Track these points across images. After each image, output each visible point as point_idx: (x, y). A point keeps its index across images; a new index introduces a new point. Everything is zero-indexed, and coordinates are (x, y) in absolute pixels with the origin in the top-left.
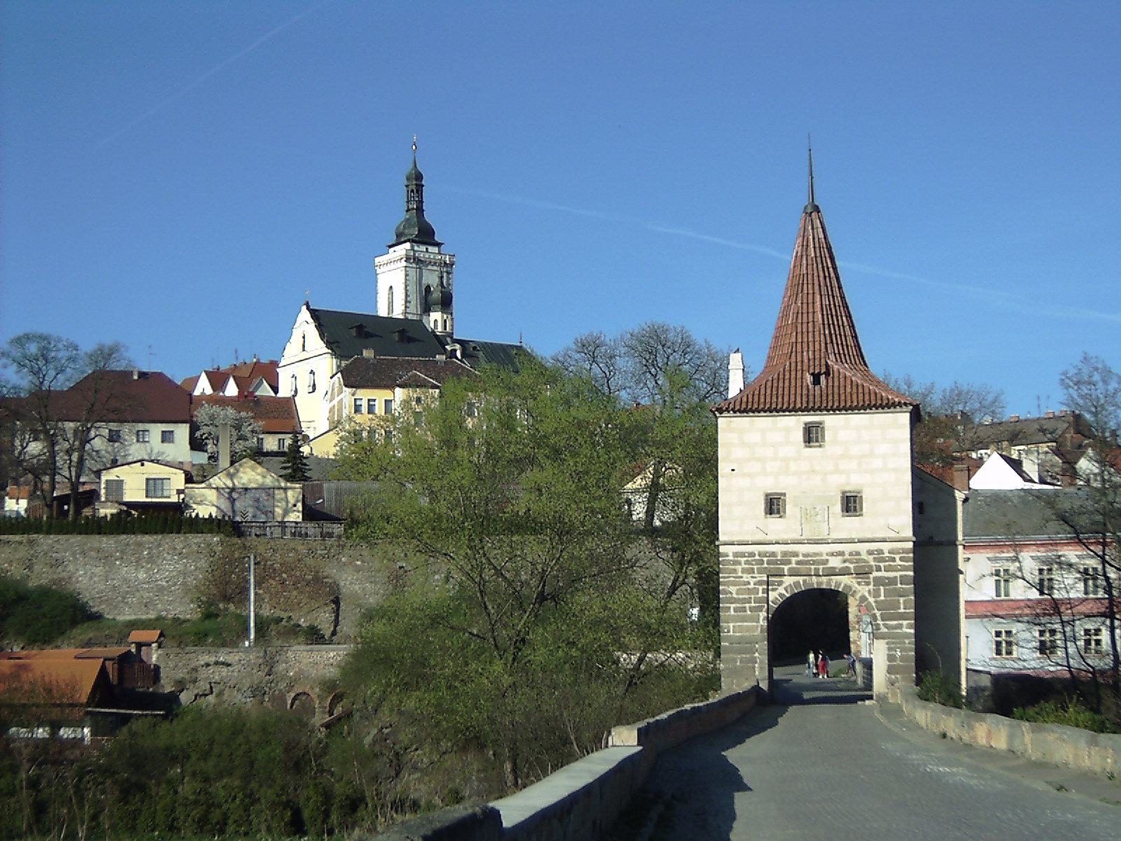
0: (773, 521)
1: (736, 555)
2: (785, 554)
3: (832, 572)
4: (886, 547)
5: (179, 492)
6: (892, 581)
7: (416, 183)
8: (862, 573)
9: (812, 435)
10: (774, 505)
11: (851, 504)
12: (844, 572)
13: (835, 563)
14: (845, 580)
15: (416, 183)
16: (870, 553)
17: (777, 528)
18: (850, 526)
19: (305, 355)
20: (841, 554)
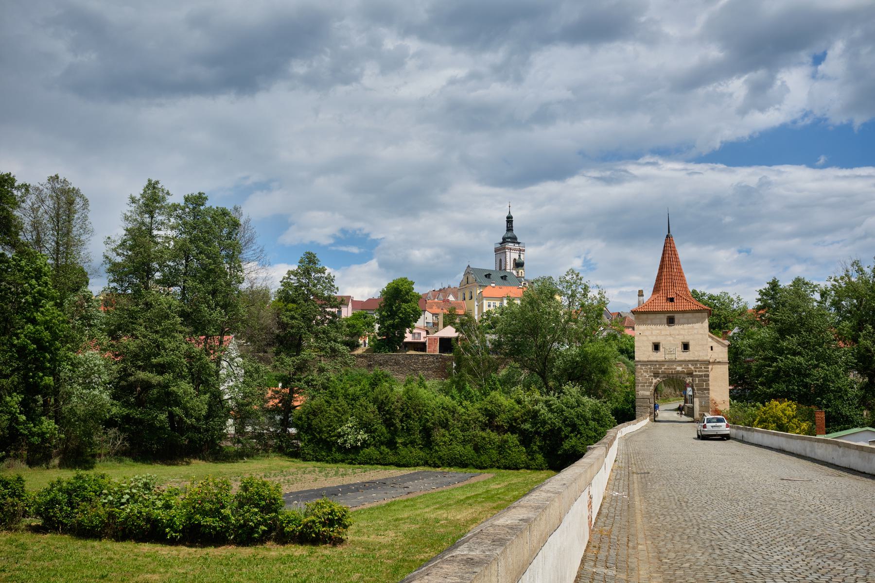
6: (701, 376)
10: (656, 347)
11: (686, 347)
17: (659, 356)
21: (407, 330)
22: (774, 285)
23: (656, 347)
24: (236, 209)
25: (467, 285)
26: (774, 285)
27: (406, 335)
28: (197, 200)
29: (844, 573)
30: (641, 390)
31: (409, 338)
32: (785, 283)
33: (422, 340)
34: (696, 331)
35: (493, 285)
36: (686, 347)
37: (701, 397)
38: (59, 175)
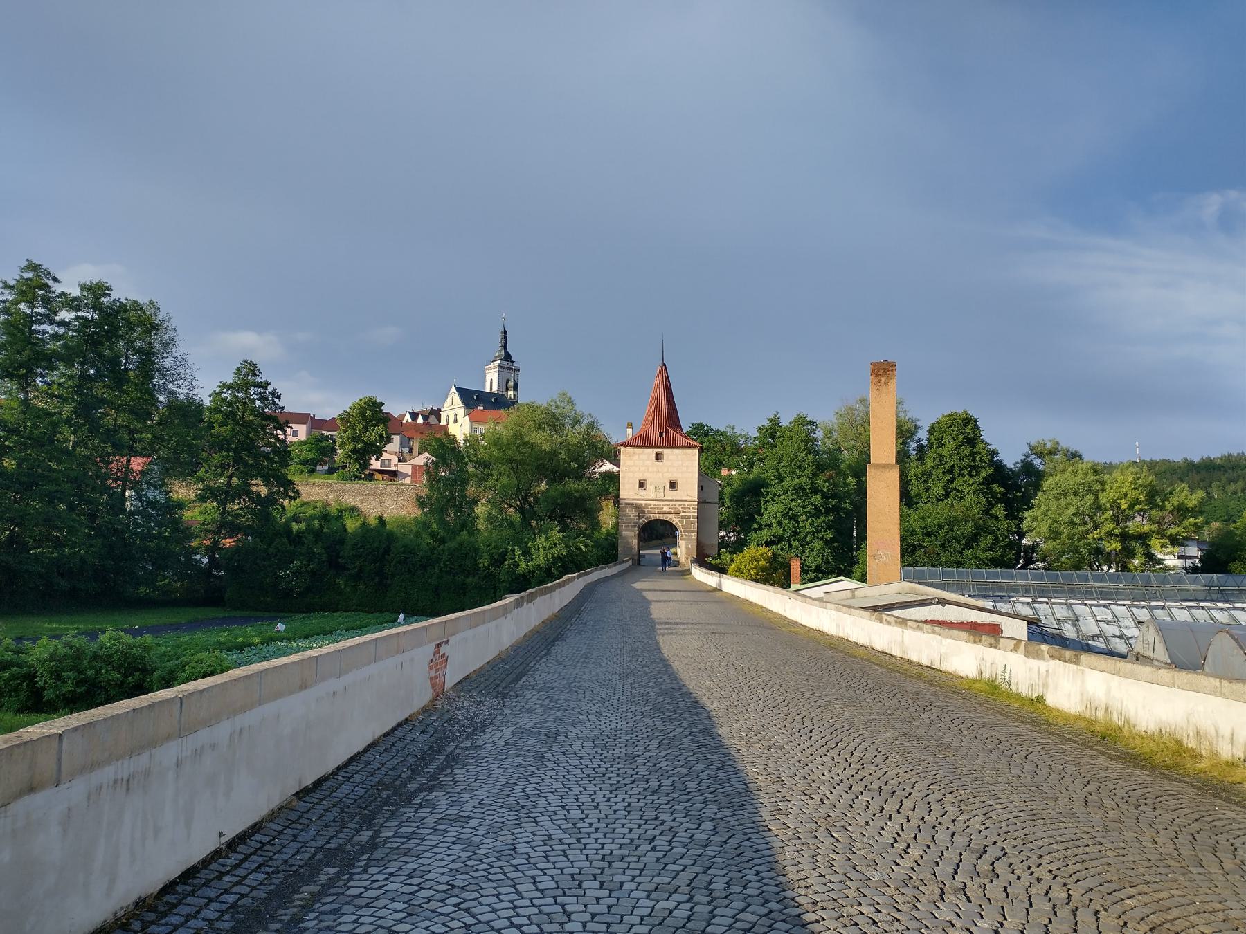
2: (646, 504)
3: (664, 513)
4: (686, 503)
5: (395, 466)
6: (689, 517)
8: (677, 513)
10: (642, 485)
12: (670, 513)
13: (666, 509)
14: (670, 516)
16: (680, 505)
18: (671, 494)
19: (453, 407)
20: (668, 505)
21: (374, 458)
22: (775, 422)
23: (642, 485)
24: (152, 303)
25: (453, 407)
26: (775, 422)
27: (371, 462)
28: (98, 290)
29: (646, 804)
30: (626, 530)
31: (375, 465)
32: (786, 420)
33: (393, 469)
34: (685, 469)
35: (481, 408)
36: (673, 485)
37: (688, 540)
38: (36, 261)
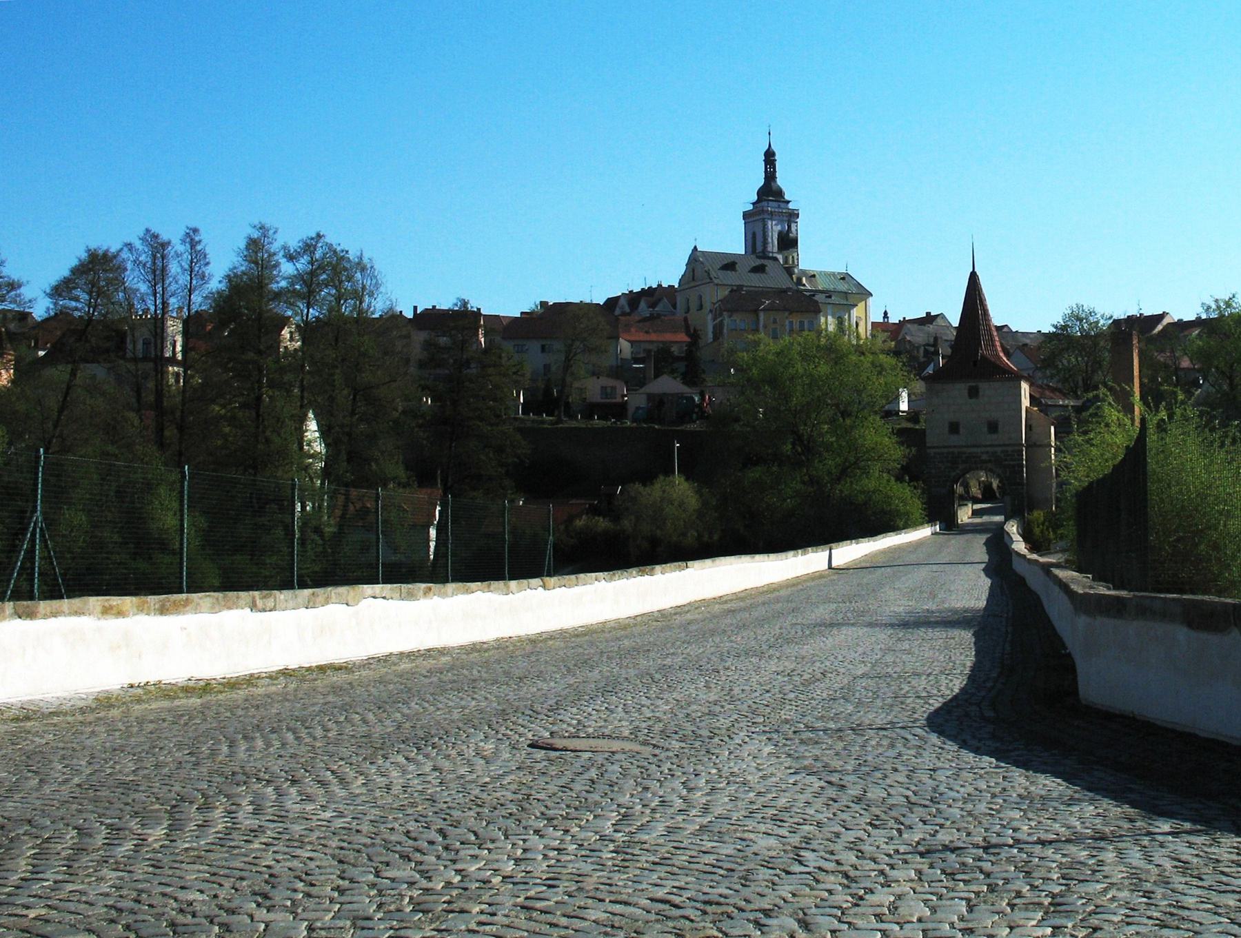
0: (995, 436)
1: (935, 453)
4: (1010, 449)
7: (770, 157)
9: (973, 393)
15: (770, 157)
20: (987, 452)
